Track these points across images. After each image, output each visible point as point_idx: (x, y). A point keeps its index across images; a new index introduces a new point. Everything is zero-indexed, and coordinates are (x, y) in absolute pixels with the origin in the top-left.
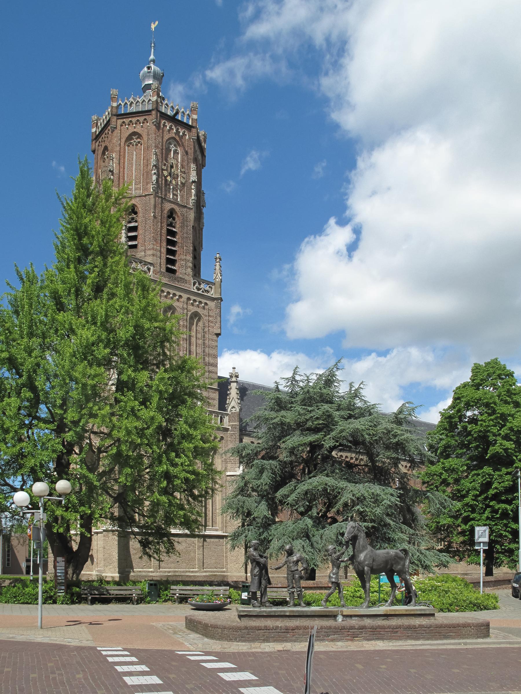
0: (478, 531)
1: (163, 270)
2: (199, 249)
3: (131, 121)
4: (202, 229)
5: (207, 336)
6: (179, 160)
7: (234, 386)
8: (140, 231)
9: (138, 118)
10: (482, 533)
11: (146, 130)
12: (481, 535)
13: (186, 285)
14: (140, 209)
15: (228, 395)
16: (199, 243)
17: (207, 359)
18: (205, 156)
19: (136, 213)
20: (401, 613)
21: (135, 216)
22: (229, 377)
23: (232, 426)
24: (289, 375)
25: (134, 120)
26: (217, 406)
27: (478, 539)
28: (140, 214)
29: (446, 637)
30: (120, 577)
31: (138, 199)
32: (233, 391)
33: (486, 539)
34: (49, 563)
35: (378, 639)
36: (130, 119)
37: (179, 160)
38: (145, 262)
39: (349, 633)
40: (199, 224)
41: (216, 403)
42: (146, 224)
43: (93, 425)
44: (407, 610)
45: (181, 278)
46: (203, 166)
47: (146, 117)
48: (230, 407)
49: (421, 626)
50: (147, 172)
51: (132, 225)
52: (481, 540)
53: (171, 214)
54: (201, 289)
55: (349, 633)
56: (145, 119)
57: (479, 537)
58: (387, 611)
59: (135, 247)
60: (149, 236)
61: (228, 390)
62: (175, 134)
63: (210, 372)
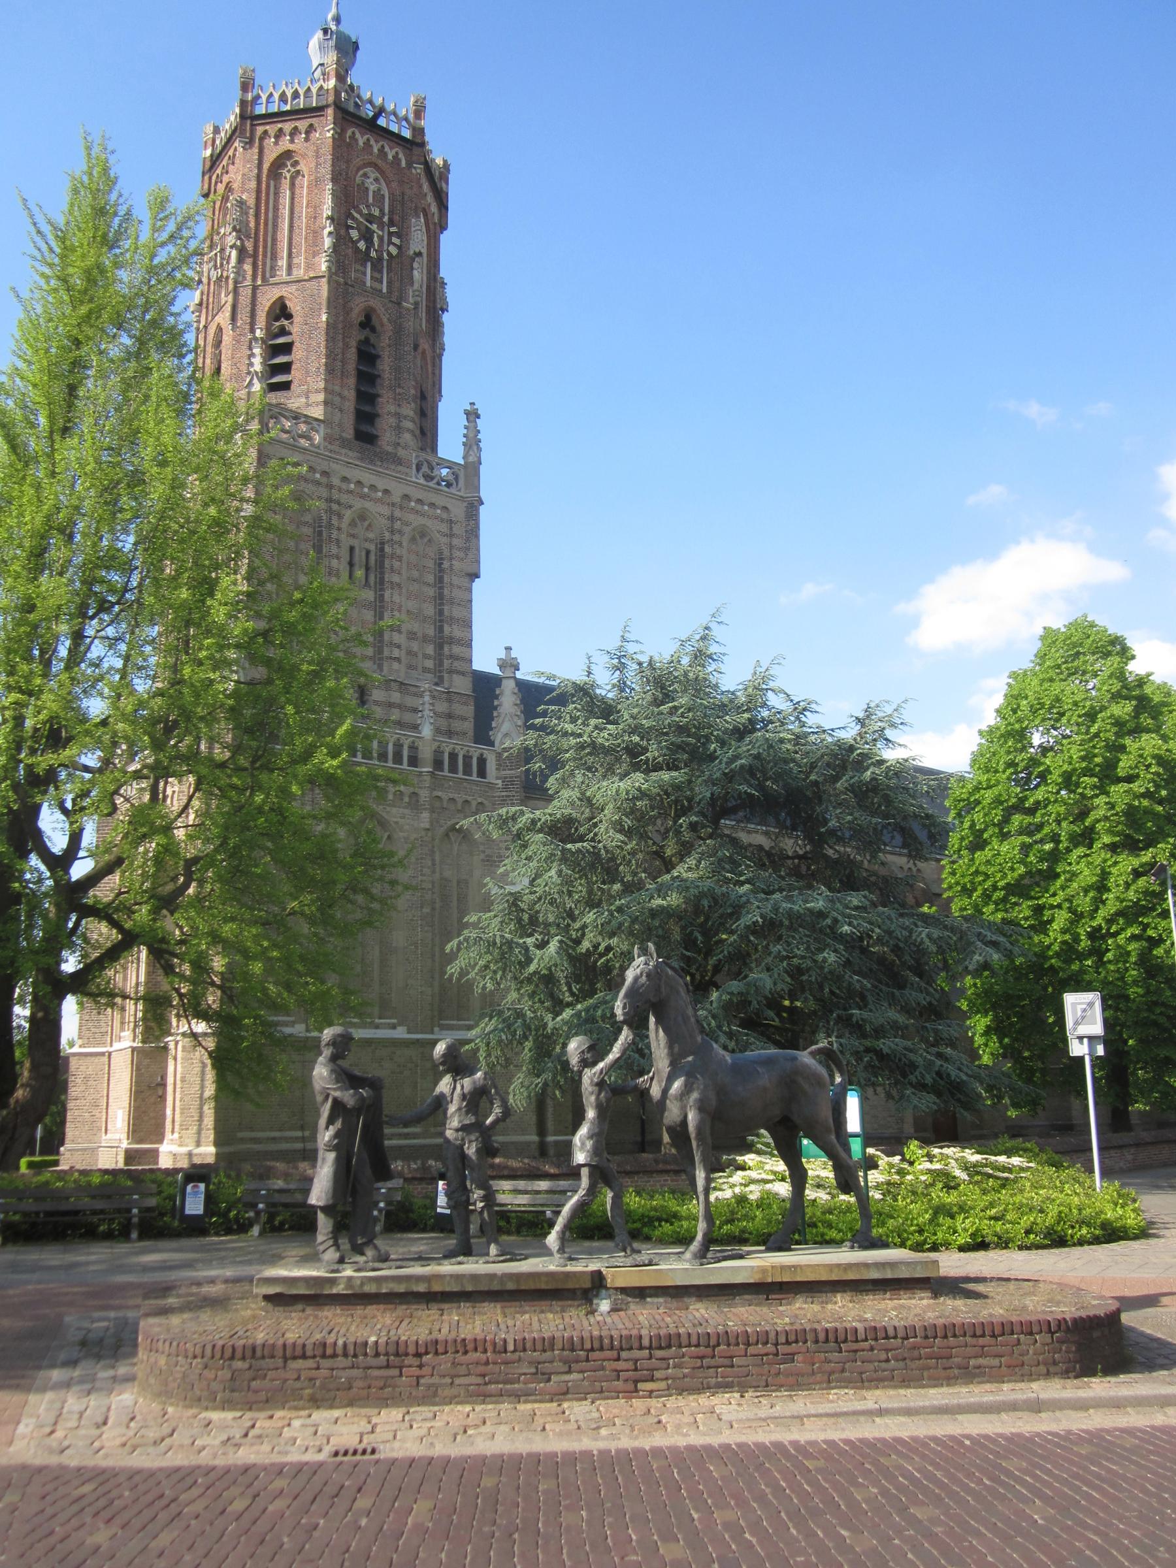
0: (1074, 1005)
1: (349, 433)
2: (433, 396)
3: (281, 130)
4: (440, 356)
5: (446, 579)
6: (386, 210)
7: (508, 686)
9: (298, 124)
10: (1084, 1010)
11: (313, 148)
12: (1083, 1018)
13: (400, 468)
14: (293, 306)
15: (496, 708)
16: (434, 385)
17: (447, 629)
18: (447, 208)
19: (289, 316)
20: (811, 1277)
21: (286, 322)
22: (496, 671)
24: (613, 644)
25: (288, 127)
26: (471, 733)
27: (1075, 1029)
28: (297, 319)
29: (969, 1375)
30: (217, 1154)
31: (294, 287)
32: (508, 701)
33: (1097, 1029)
34: (68, 1125)
35: (726, 1386)
36: (279, 126)
37: (386, 210)
38: (306, 416)
39: (621, 1365)
40: (433, 346)
41: (469, 726)
42: (310, 338)
44: (831, 1267)
45: (388, 453)
46: (443, 227)
47: (314, 121)
48: (500, 736)
49: (876, 1333)
50: (315, 232)
51: (281, 340)
52: (1083, 1030)
53: (367, 323)
54: (432, 478)
55: (621, 1365)
56: (311, 126)
57: (1077, 1023)
58: (763, 1270)
59: (286, 386)
60: (318, 361)
61: (497, 697)
63: (457, 658)
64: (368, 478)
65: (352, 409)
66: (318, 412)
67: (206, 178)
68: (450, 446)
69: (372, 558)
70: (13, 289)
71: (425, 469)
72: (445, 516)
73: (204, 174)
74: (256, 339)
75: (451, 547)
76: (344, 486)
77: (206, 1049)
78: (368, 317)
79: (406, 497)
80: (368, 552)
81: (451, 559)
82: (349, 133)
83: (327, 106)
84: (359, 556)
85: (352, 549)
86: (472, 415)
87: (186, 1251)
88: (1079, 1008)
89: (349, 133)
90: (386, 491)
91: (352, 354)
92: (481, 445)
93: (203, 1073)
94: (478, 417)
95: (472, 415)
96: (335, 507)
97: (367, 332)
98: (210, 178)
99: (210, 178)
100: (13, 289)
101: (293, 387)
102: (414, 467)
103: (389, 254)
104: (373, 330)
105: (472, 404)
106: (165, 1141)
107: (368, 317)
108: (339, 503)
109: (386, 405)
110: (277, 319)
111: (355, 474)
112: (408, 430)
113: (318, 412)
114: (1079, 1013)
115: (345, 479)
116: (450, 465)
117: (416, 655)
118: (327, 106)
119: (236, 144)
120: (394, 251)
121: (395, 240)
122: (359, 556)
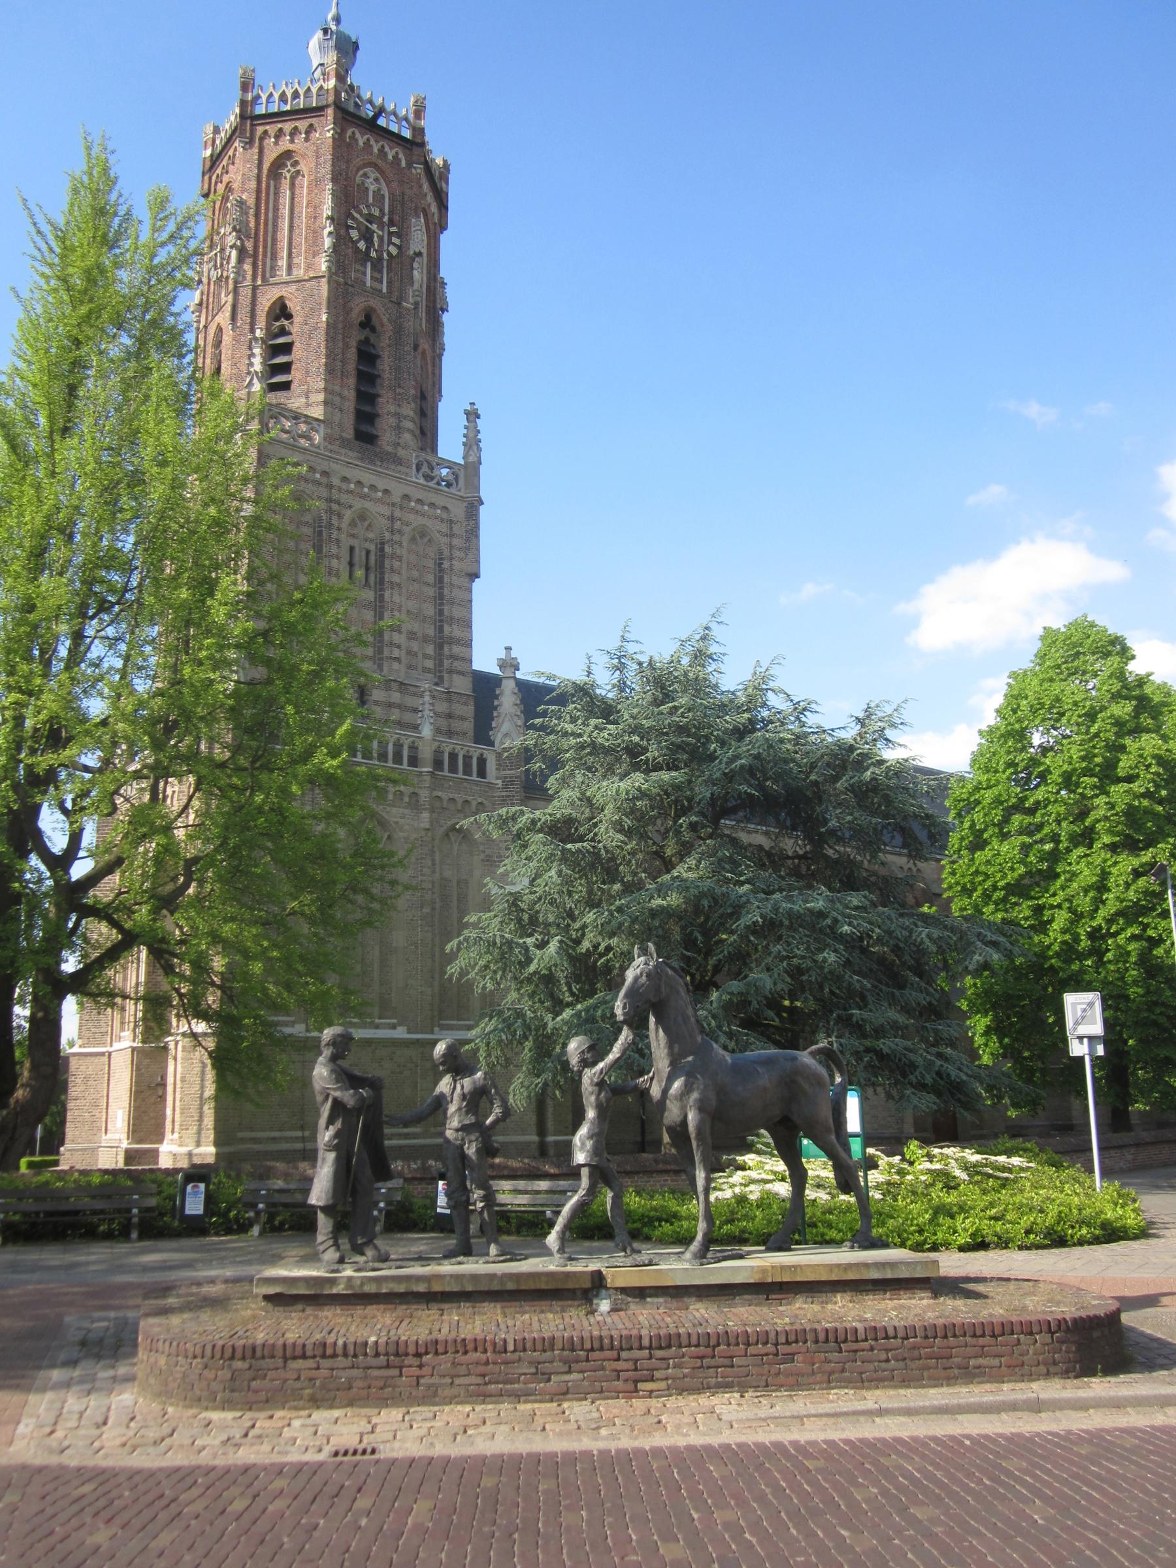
0: (1074, 1005)
1: (349, 433)
2: (433, 396)
4: (440, 356)
5: (446, 579)
6: (386, 210)
7: (508, 686)
8: (298, 354)
9: (298, 124)
10: (1084, 1010)
11: (313, 148)
12: (1083, 1018)
13: (400, 468)
14: (293, 306)
15: (496, 708)
16: (434, 385)
17: (447, 629)
18: (447, 208)
19: (289, 316)
20: (811, 1277)
21: (286, 322)
22: (496, 671)
23: (504, 779)
24: (613, 644)
25: (288, 127)
26: (471, 733)
27: (1075, 1029)
28: (297, 319)
29: (969, 1375)
30: (217, 1154)
31: (294, 287)
32: (508, 701)
33: (1097, 1029)
34: (68, 1125)
36: (279, 126)
37: (386, 210)
38: (306, 416)
39: (621, 1365)
40: (433, 346)
42: (310, 338)
43: (410, 851)
44: (831, 1267)
45: (388, 453)
46: (443, 227)
47: (314, 121)
48: (500, 736)
49: (876, 1333)
50: (315, 232)
51: (281, 340)
52: (1083, 1030)
53: (367, 323)
54: (432, 478)
55: (621, 1365)
56: (311, 126)
57: (1077, 1023)
58: (763, 1270)
59: (286, 386)
60: (318, 361)
61: (497, 697)
62: (378, 156)
63: (457, 658)
64: (368, 478)
65: (352, 409)
66: (318, 412)
67: (206, 178)
68: (450, 446)
69: (372, 558)
70: (13, 289)
71: (425, 469)
72: (445, 516)
73: (204, 174)
74: (256, 339)
75: (451, 547)
76: (344, 486)
77: (206, 1049)
78: (368, 317)
79: (406, 497)
80: (368, 552)
81: (451, 559)
82: (349, 133)
83: (327, 106)
84: (359, 556)
85: (352, 549)
86: (472, 415)
87: (186, 1251)
88: (1079, 1008)
89: (349, 133)
90: (386, 491)
91: (352, 354)
92: (481, 445)
93: (203, 1073)
94: (478, 417)
95: (472, 415)
96: (335, 507)
97: (367, 332)
98: (210, 178)
99: (210, 178)
100: (13, 289)
101: (293, 387)
102: (414, 467)
103: (389, 254)
104: (373, 330)
105: (472, 404)
106: (165, 1141)
107: (368, 317)
108: (339, 503)
109: (386, 405)
110: (277, 319)
111: (355, 474)
112: (408, 430)
113: (318, 412)
114: (1079, 1013)
115: (345, 479)
116: (450, 465)
117: (416, 655)
118: (327, 106)
119: (236, 144)
120: (394, 251)
121: (395, 240)
122: (359, 556)
